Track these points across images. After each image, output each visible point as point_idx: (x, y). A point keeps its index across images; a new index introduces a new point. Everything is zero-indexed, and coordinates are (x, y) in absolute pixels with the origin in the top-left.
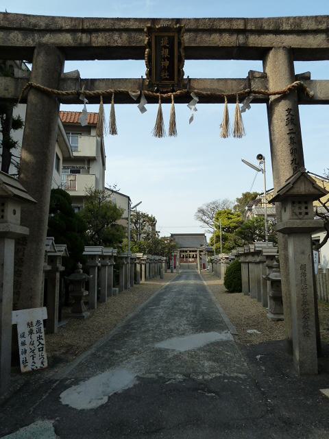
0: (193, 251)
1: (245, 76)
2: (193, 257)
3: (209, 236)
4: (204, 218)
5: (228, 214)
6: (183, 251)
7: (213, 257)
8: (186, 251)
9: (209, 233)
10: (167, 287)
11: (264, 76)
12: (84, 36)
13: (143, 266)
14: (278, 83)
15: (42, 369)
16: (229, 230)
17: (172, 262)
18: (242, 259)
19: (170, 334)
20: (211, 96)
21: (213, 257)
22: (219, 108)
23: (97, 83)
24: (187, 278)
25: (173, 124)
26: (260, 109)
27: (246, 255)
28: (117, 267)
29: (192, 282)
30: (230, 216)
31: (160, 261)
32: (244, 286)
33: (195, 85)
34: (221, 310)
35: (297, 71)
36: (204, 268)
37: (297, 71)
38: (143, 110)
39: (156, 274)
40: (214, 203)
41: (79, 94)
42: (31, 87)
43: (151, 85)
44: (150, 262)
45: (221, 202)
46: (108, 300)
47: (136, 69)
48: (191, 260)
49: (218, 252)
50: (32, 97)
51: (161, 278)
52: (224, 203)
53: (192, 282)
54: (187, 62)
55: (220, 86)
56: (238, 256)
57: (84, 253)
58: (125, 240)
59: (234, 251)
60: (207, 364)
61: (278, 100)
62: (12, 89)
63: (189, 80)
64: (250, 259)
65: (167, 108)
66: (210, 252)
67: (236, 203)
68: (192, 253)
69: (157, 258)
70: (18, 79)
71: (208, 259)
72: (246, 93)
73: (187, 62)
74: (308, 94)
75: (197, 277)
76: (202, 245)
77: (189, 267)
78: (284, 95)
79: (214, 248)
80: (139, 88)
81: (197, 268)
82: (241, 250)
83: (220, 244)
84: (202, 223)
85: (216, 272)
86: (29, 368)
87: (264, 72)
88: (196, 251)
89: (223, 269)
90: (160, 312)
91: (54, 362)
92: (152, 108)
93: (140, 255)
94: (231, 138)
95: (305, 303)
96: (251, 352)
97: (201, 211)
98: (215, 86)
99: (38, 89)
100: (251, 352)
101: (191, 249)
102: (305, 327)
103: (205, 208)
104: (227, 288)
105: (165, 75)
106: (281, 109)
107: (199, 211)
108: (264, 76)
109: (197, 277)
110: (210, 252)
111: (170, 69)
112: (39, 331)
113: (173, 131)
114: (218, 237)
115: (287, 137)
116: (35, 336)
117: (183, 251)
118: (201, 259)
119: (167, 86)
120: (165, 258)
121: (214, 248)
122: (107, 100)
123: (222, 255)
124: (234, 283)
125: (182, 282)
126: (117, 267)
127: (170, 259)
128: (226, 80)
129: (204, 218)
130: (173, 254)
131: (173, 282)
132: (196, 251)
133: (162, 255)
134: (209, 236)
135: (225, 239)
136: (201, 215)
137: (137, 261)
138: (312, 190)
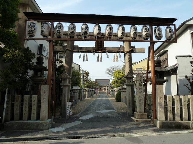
0: (104, 87)
1: (119, 46)
2: (105, 89)
3: (111, 81)
4: (109, 73)
5: (119, 73)
6: (101, 87)
7: (112, 89)
8: (102, 87)
9: (111, 79)
10: (95, 100)
11: (123, 47)
12: (80, 36)
13: (86, 93)
14: (127, 49)
15: (71, 115)
16: (119, 79)
17: (96, 91)
18: (121, 90)
19: (99, 110)
20: (111, 51)
21: (112, 89)
22: (113, 54)
23: (83, 48)
24: (102, 97)
25: (101, 59)
26: (123, 54)
27: (122, 89)
28: (80, 93)
29: (104, 98)
30: (119, 73)
31: (92, 91)
32: (122, 101)
33: (106, 49)
34: (113, 106)
35: (132, 45)
36: (109, 93)
37: (132, 45)
38: (94, 55)
39: (91, 96)
40: (113, 67)
41: (79, 51)
42: (67, 49)
43: (96, 49)
44: (89, 91)
45: (116, 66)
46: (78, 103)
47: (92, 44)
48: (104, 90)
49: (114, 87)
50: (67, 51)
51: (93, 97)
52: (118, 67)
53: (104, 98)
54: (105, 42)
55: (113, 49)
56: (120, 89)
57: (73, 88)
58: (81, 83)
59: (119, 88)
60: (108, 114)
61: (126, 53)
62: (62, 49)
63: (105, 47)
64: (123, 90)
65: (100, 54)
66: (111, 87)
67: (123, 67)
68: (104, 88)
69: (91, 89)
70: (63, 47)
71: (110, 90)
72: (119, 50)
73: (105, 42)
74: (134, 51)
75: (106, 97)
76: (108, 84)
77: (103, 93)
78: (128, 52)
79: (113, 86)
80: (93, 50)
81: (106, 93)
82: (121, 87)
83: (115, 84)
84: (108, 75)
85: (113, 95)
86: (69, 115)
87: (124, 46)
88: (106, 87)
89: (116, 93)
90: (95, 106)
91: (73, 115)
92: (96, 54)
93: (86, 88)
94: (115, 62)
95: (129, 101)
96: (119, 114)
97: (108, 70)
98: (112, 49)
99: (69, 50)
100: (119, 114)
101: (104, 86)
102: (129, 106)
103: (110, 69)
104: (117, 100)
105: (100, 47)
106: (127, 55)
107: (107, 70)
108: (123, 47)
109: (106, 97)
110: (111, 87)
111: (101, 46)
112: (70, 107)
113: (101, 61)
114: (114, 81)
115: (128, 62)
116: (70, 108)
117: (101, 87)
118: (108, 90)
119: (100, 49)
120: (93, 90)
121: (113, 86)
122: (85, 52)
123: (115, 89)
124: (119, 98)
125: (100, 98)
126: (80, 93)
127: (95, 90)
128: (114, 48)
129: (109, 73)
130: (97, 88)
131: (97, 99)
132: (106, 87)
133: (92, 88)
134: (111, 81)
135: (117, 82)
136: (108, 71)
137: (85, 91)
138: (131, 77)
